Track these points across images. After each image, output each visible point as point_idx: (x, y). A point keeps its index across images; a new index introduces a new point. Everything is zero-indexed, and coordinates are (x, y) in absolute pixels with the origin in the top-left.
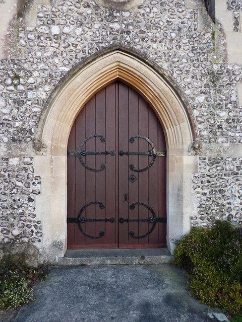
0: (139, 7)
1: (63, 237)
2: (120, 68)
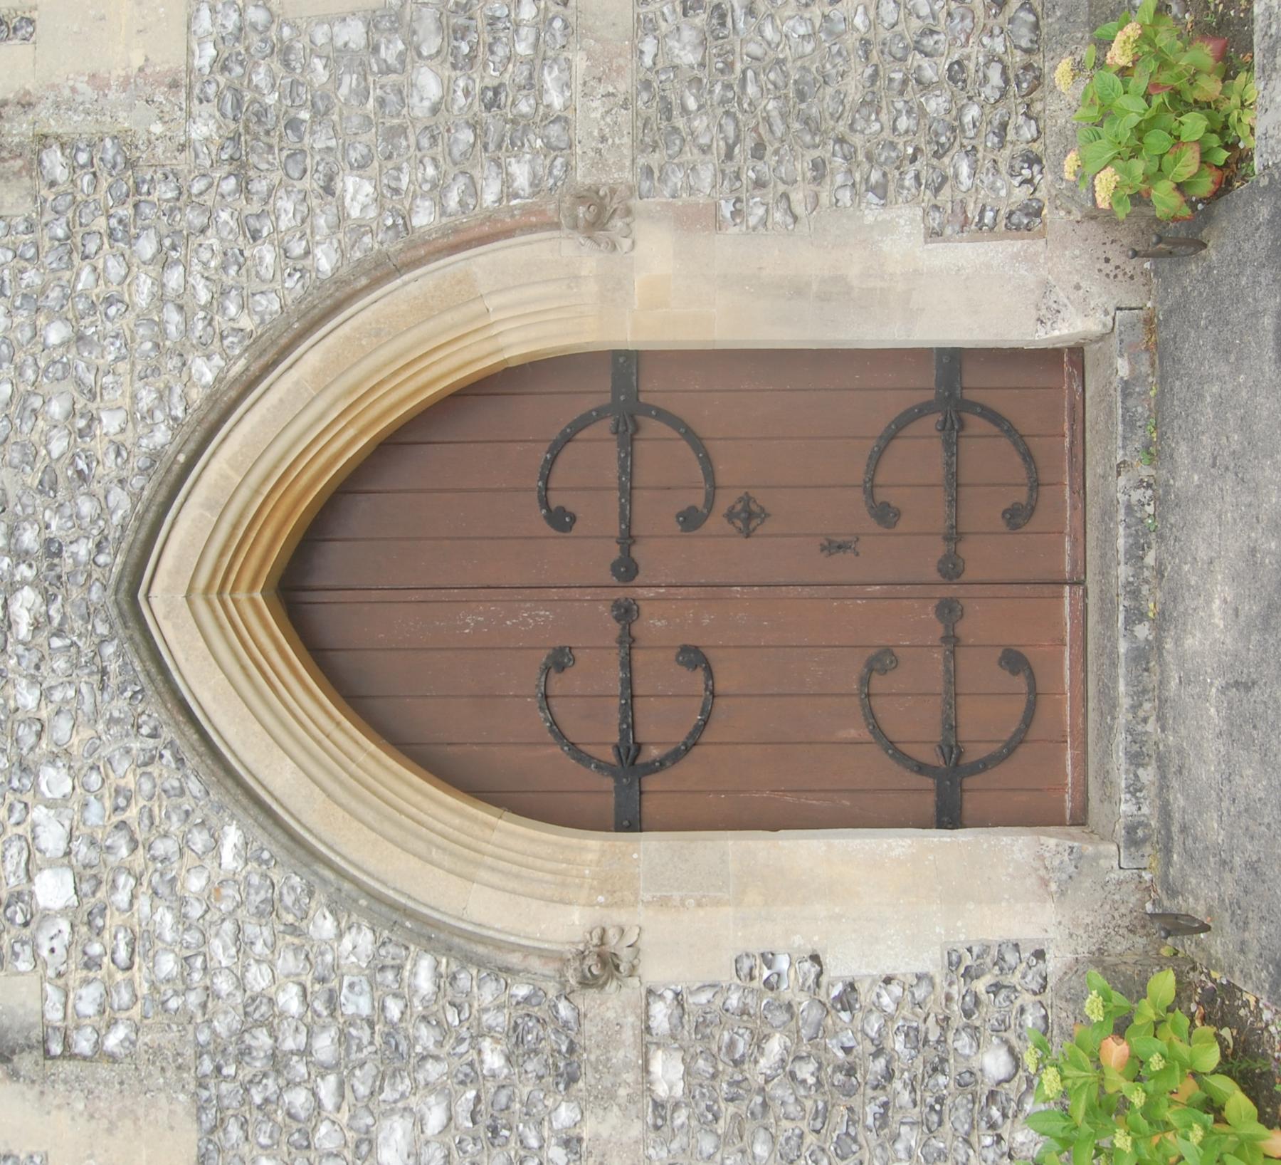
1: (1013, 849)
2: (220, 586)
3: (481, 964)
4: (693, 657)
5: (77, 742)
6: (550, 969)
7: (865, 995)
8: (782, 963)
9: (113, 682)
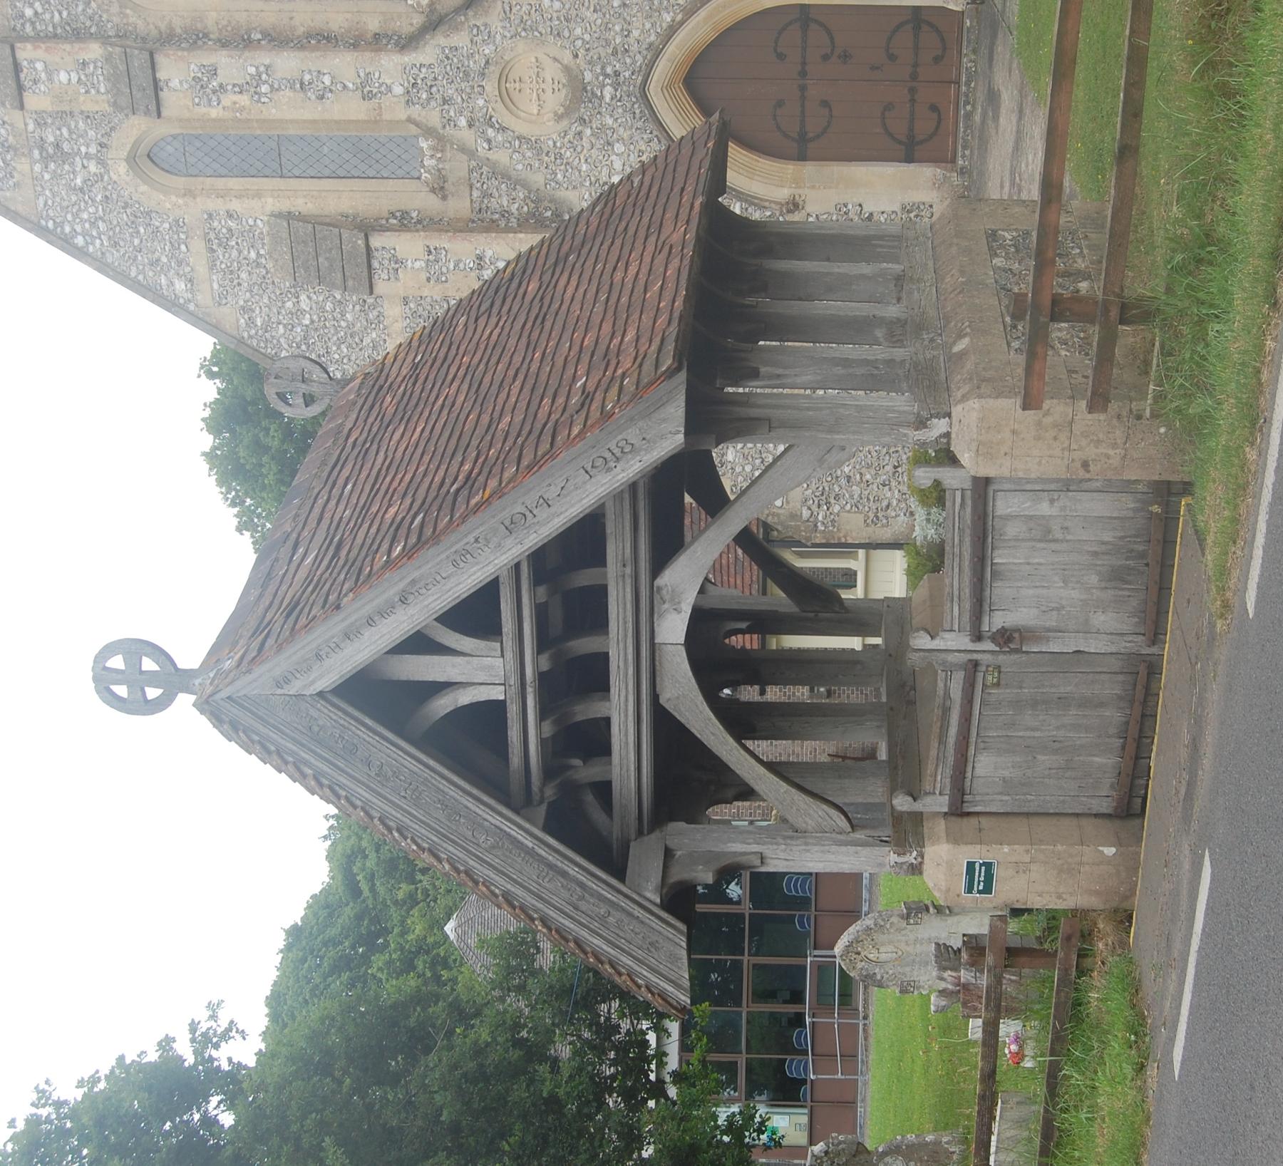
0: (576, 56)
1: (927, 172)
2: (669, 86)
3: (755, 205)
4: (825, 104)
5: (625, 136)
6: (778, 207)
7: (876, 217)
8: (850, 207)
9: (638, 116)
